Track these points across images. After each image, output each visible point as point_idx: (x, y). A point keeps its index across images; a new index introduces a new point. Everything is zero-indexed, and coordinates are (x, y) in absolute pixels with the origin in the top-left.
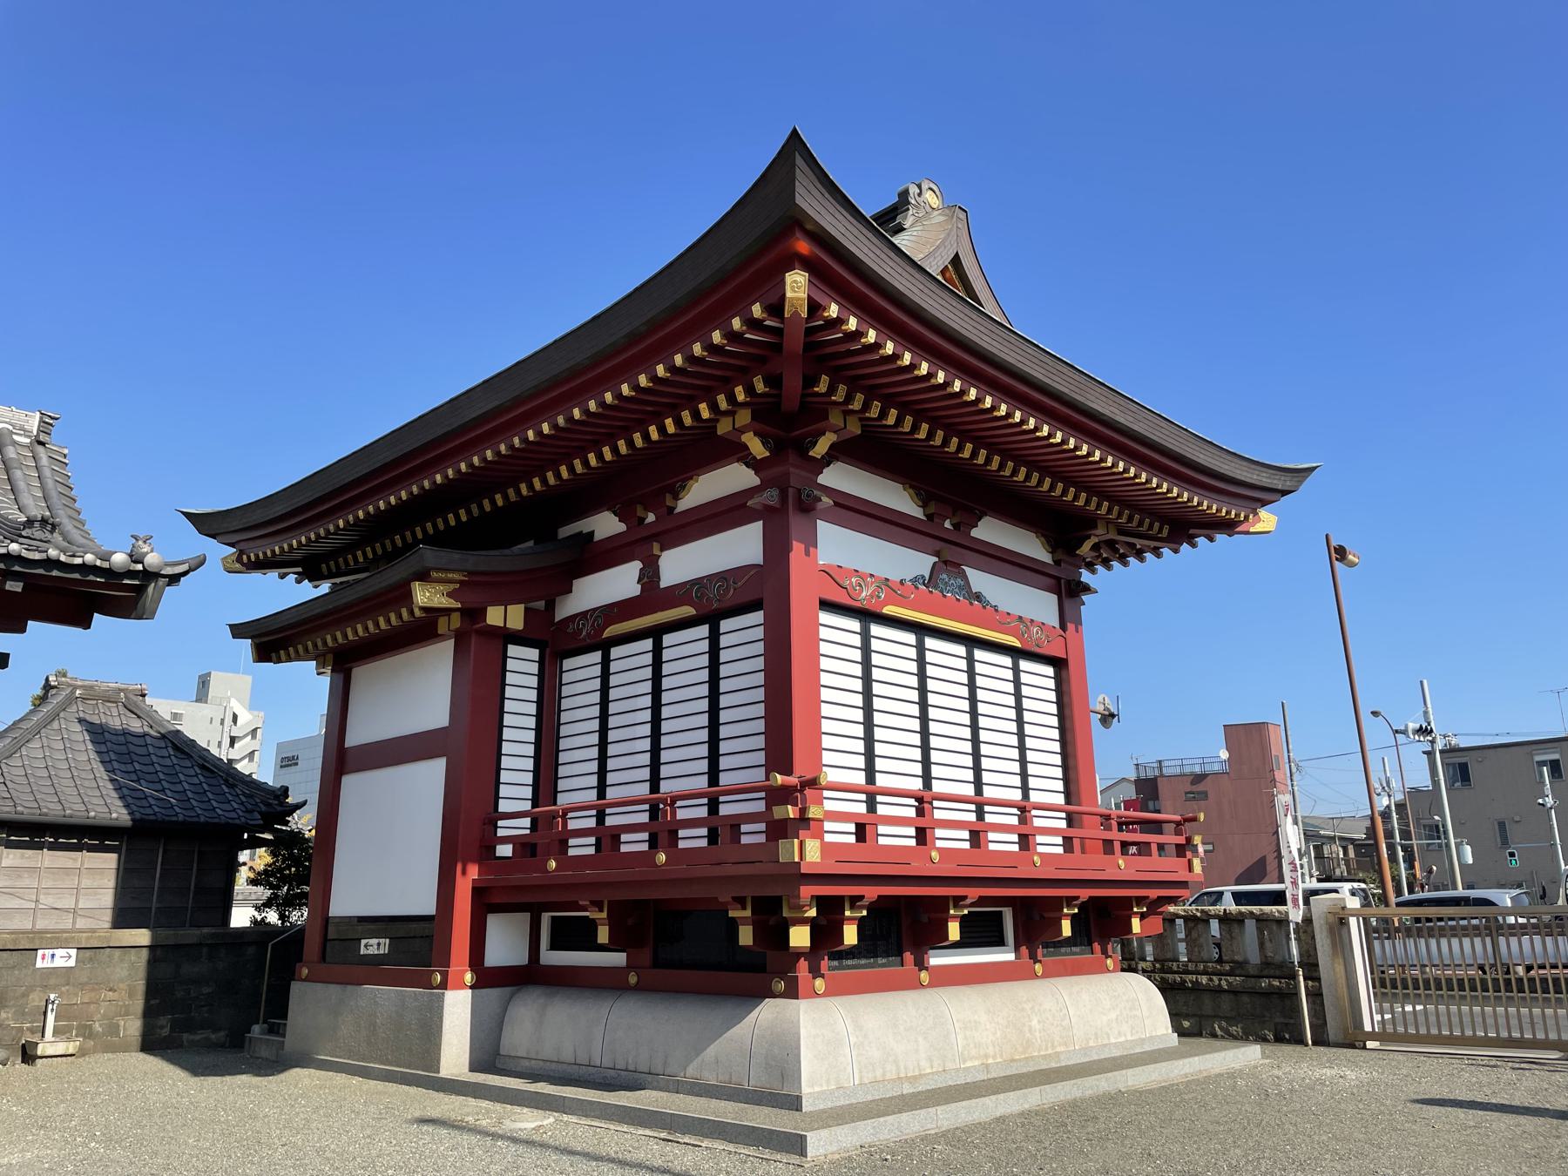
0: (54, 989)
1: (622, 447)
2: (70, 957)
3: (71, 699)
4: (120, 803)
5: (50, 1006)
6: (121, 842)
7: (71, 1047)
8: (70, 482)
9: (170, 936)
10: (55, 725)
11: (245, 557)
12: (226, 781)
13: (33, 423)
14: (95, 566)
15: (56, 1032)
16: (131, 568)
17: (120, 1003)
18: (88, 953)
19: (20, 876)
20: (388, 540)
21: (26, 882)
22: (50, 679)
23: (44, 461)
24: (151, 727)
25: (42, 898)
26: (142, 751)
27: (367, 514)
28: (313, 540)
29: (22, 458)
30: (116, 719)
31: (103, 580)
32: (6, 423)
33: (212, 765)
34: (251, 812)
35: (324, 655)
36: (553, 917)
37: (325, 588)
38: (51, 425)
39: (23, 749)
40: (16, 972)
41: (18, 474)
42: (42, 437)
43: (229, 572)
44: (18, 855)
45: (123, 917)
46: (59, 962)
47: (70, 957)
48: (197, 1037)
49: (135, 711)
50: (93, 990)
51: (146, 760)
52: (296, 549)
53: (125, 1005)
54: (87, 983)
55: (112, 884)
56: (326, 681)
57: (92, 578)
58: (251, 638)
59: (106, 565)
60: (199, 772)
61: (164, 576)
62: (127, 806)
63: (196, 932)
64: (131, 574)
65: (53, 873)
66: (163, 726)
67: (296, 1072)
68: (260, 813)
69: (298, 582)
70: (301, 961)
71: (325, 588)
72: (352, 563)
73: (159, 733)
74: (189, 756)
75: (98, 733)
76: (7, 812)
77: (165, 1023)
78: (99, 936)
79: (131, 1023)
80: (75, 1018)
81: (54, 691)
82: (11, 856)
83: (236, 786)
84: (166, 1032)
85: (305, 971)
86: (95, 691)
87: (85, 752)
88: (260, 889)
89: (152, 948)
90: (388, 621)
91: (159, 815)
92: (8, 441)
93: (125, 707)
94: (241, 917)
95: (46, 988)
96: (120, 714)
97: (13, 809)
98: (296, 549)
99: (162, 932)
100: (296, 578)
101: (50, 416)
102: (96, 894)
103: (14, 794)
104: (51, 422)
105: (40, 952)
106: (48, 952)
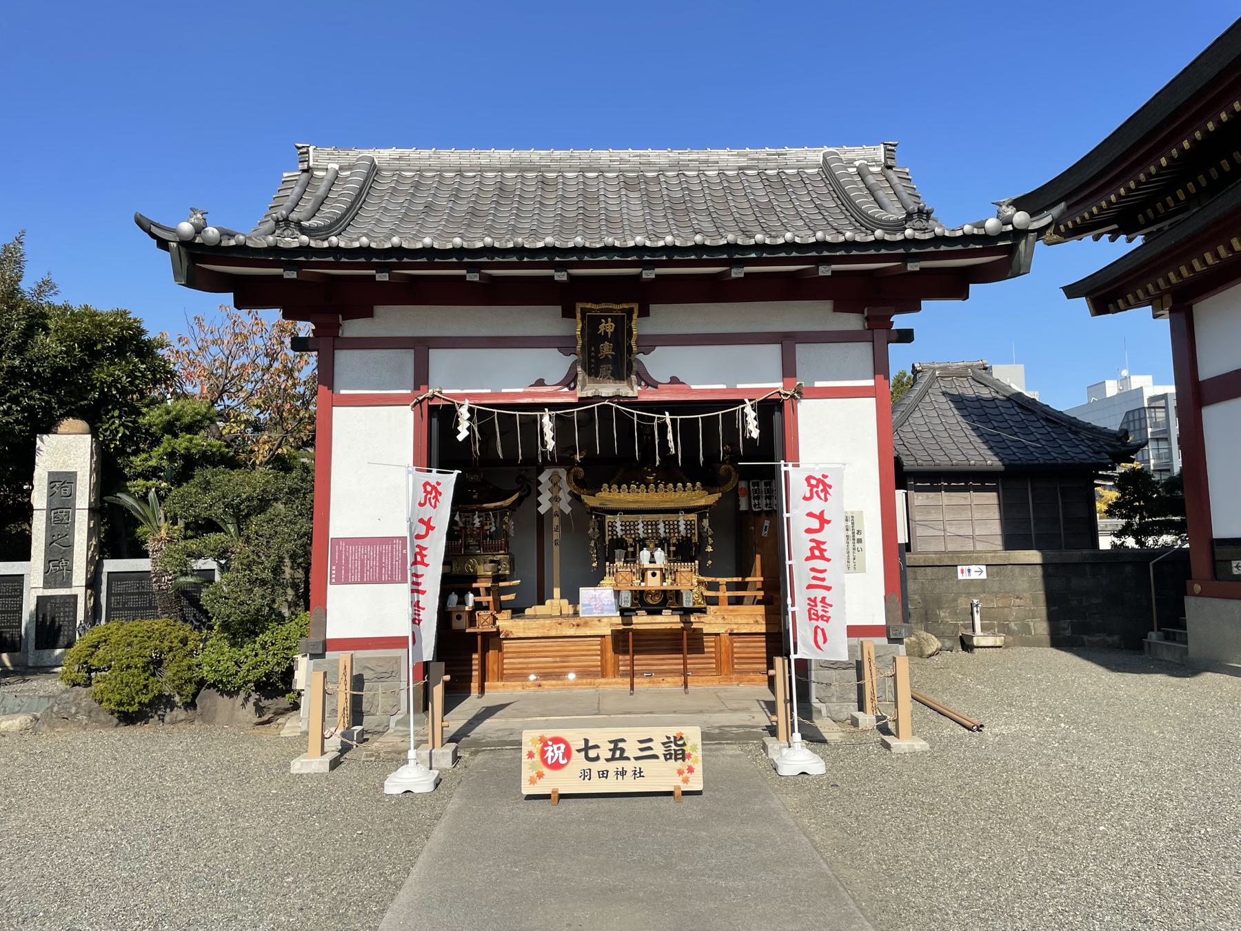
0: (975, 595)
1: (1214, 173)
2: (982, 572)
3: (934, 379)
4: (989, 453)
5: (975, 609)
6: (997, 484)
7: (999, 641)
8: (916, 193)
9: (1057, 556)
10: (927, 399)
11: (1062, 227)
12: (1070, 429)
13: (880, 153)
14: (974, 234)
15: (983, 628)
16: (1003, 230)
17: (1028, 608)
18: (995, 569)
19: (928, 512)
20: (1149, 209)
21: (934, 516)
22: (916, 366)
23: (896, 180)
24: (997, 392)
25: (948, 527)
26: (995, 412)
27: (1194, 141)
28: (1154, 173)
29: (879, 183)
30: (969, 390)
31: (981, 247)
32: (861, 159)
33: (1055, 418)
34: (1099, 453)
35: (1160, 297)
36: (408, 637)
37: (1139, 241)
38: (893, 151)
39: (909, 419)
40: (945, 582)
41: (880, 194)
42: (890, 162)
43: (1049, 245)
44: (925, 497)
45: (1013, 540)
46: (974, 576)
47: (982, 572)
48: (1095, 639)
49: (982, 381)
50: (1004, 597)
51: (1000, 418)
52: (1106, 210)
53: (1030, 610)
54: (999, 592)
55: (997, 515)
56: (1164, 323)
57: (972, 246)
58: (1086, 295)
59: (982, 232)
60: (1044, 424)
61: (1033, 231)
62: (996, 455)
63: (1078, 553)
64: (1003, 235)
65: (953, 509)
66: (1007, 390)
67: (1208, 676)
68: (1107, 453)
69: (1112, 240)
70: (1190, 578)
71: (1139, 241)
72: (1172, 204)
73: (1005, 396)
74: (1033, 412)
75: (960, 402)
76: (912, 465)
77: (1065, 625)
78: (1000, 556)
79: (1039, 624)
80: (994, 619)
81: (920, 374)
82: (920, 498)
83: (1079, 433)
84: (1068, 633)
85: (1197, 588)
86: (949, 370)
87: (953, 416)
88: (1115, 521)
89: (1044, 565)
90: (1179, 275)
91: (1024, 461)
92: (867, 173)
93: (973, 379)
94: (1105, 543)
95: (969, 594)
96: (971, 386)
97: (915, 463)
98: (1106, 210)
99: (1050, 553)
100: (1110, 238)
101: (890, 145)
102: (986, 524)
103: (913, 452)
104: (893, 148)
105: (959, 568)
106: (965, 568)
